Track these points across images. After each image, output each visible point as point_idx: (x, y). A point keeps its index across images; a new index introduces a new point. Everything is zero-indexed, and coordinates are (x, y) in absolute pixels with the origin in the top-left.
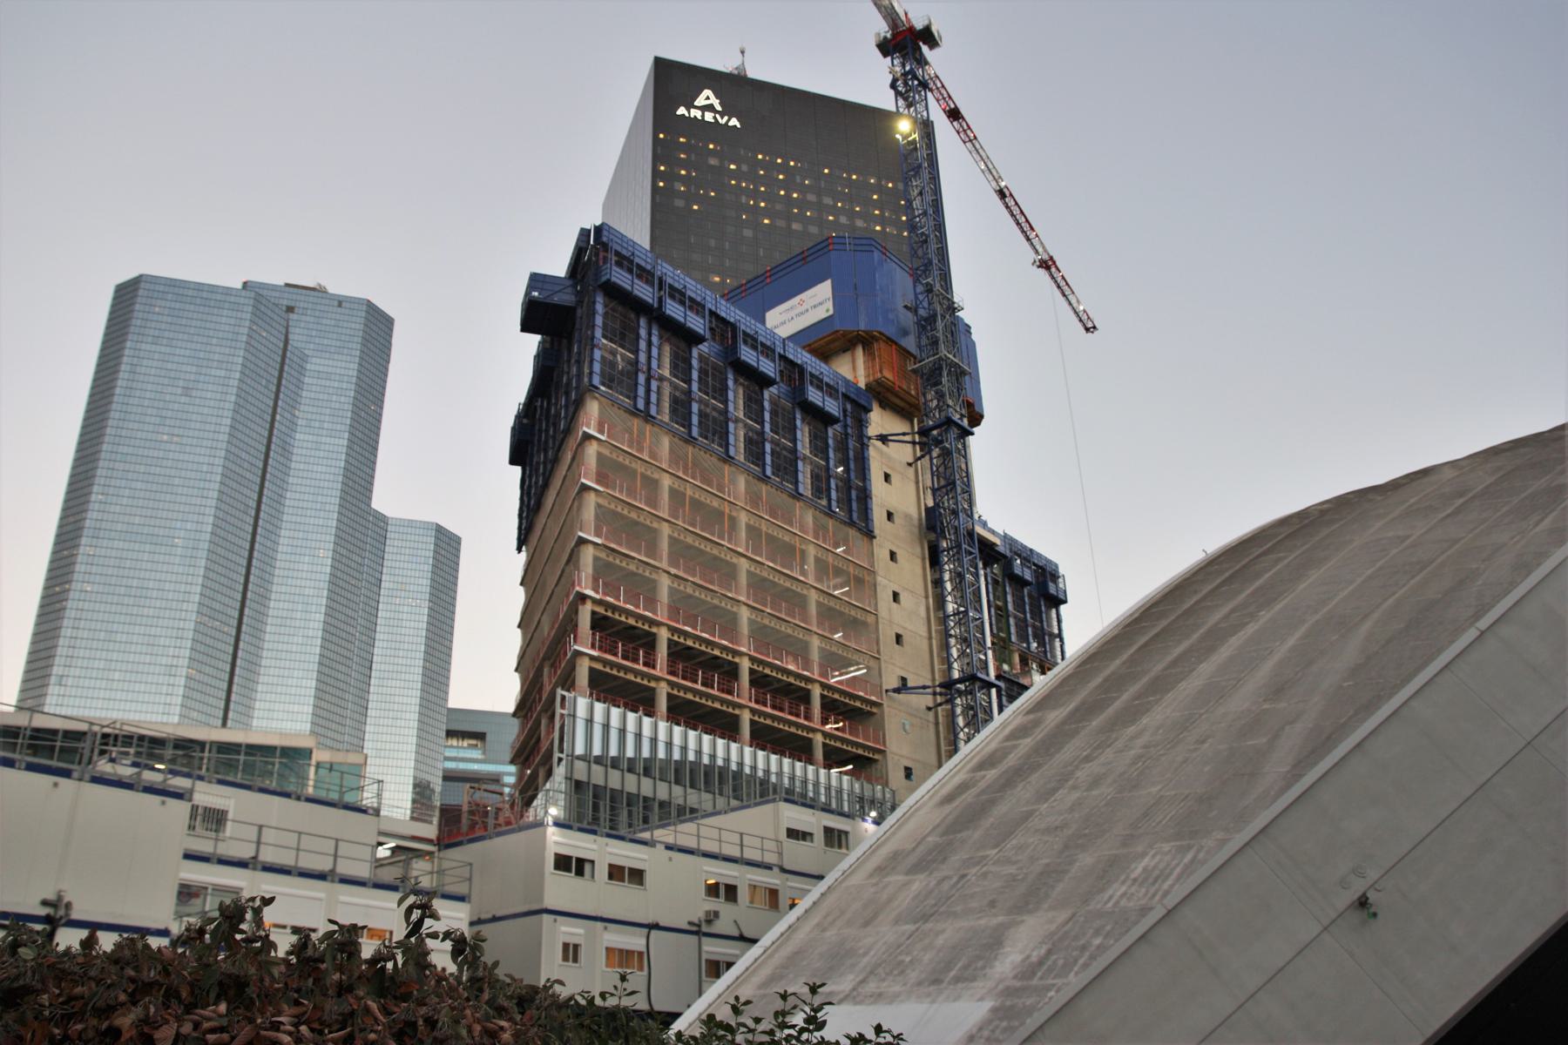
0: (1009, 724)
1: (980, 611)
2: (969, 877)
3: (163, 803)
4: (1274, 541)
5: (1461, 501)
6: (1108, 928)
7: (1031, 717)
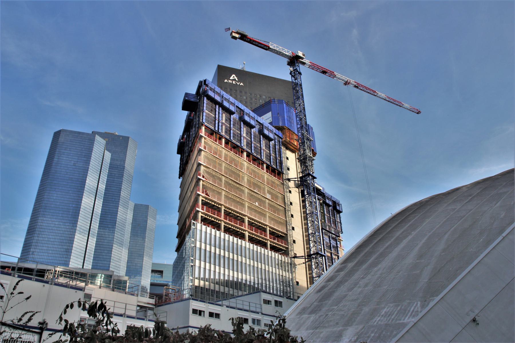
0: (336, 267)
1: (319, 233)
2: (329, 315)
3: (76, 292)
4: (413, 210)
5: (471, 198)
6: (376, 330)
7: (343, 265)
